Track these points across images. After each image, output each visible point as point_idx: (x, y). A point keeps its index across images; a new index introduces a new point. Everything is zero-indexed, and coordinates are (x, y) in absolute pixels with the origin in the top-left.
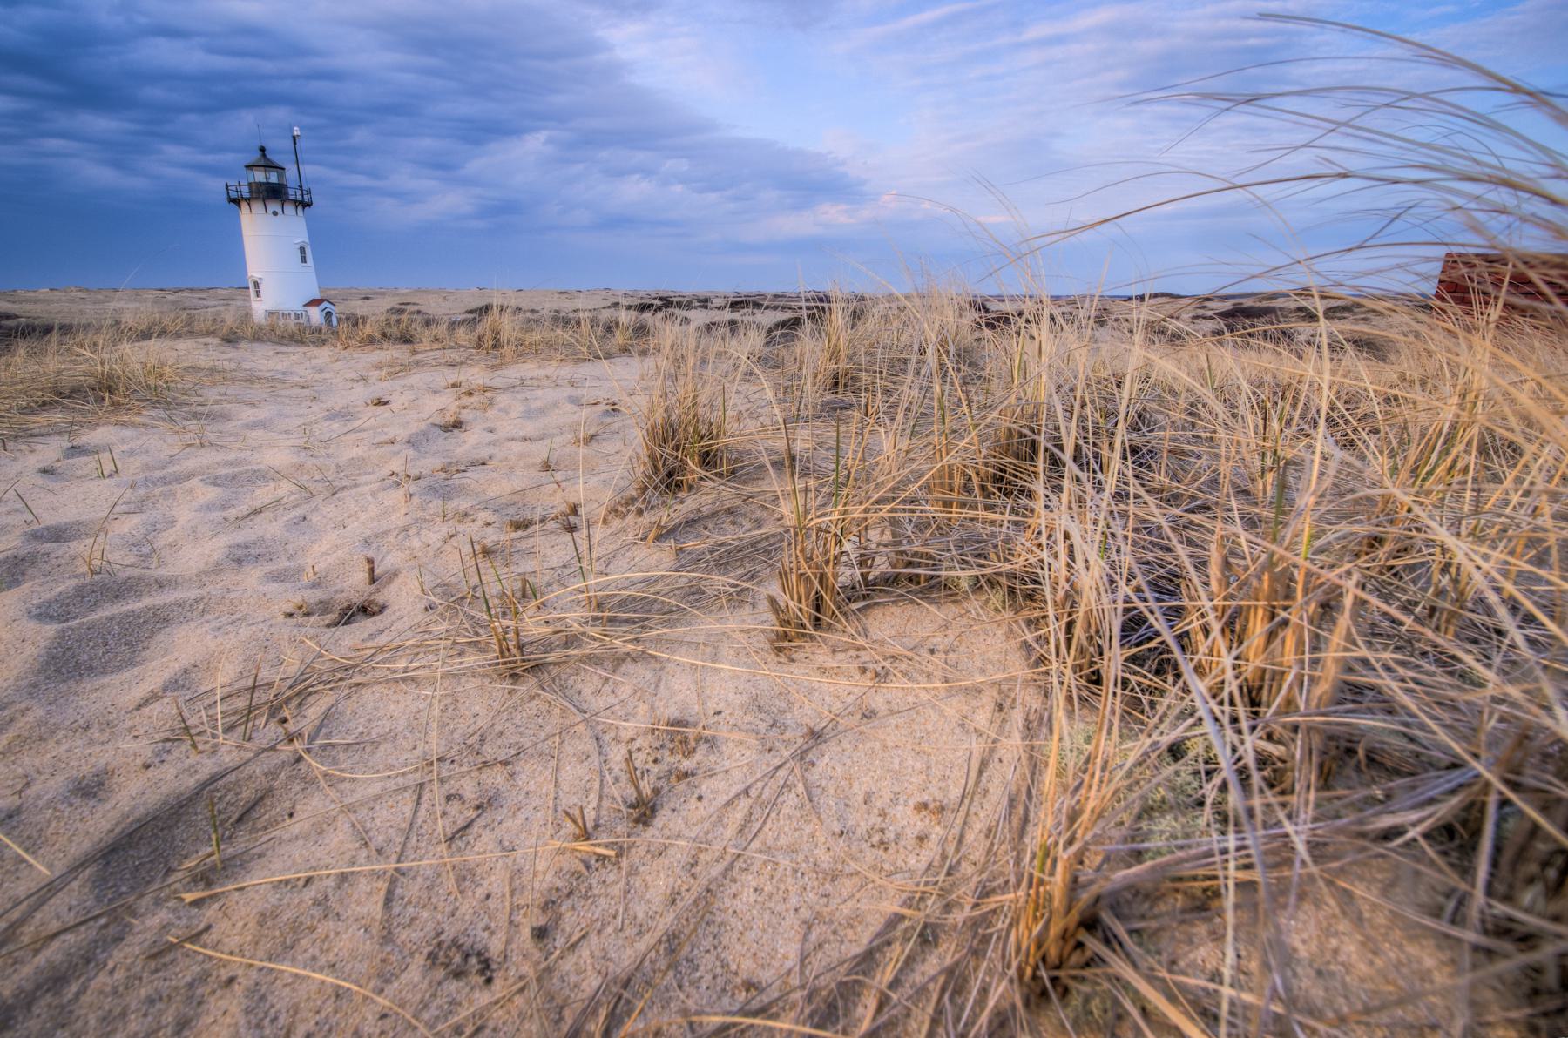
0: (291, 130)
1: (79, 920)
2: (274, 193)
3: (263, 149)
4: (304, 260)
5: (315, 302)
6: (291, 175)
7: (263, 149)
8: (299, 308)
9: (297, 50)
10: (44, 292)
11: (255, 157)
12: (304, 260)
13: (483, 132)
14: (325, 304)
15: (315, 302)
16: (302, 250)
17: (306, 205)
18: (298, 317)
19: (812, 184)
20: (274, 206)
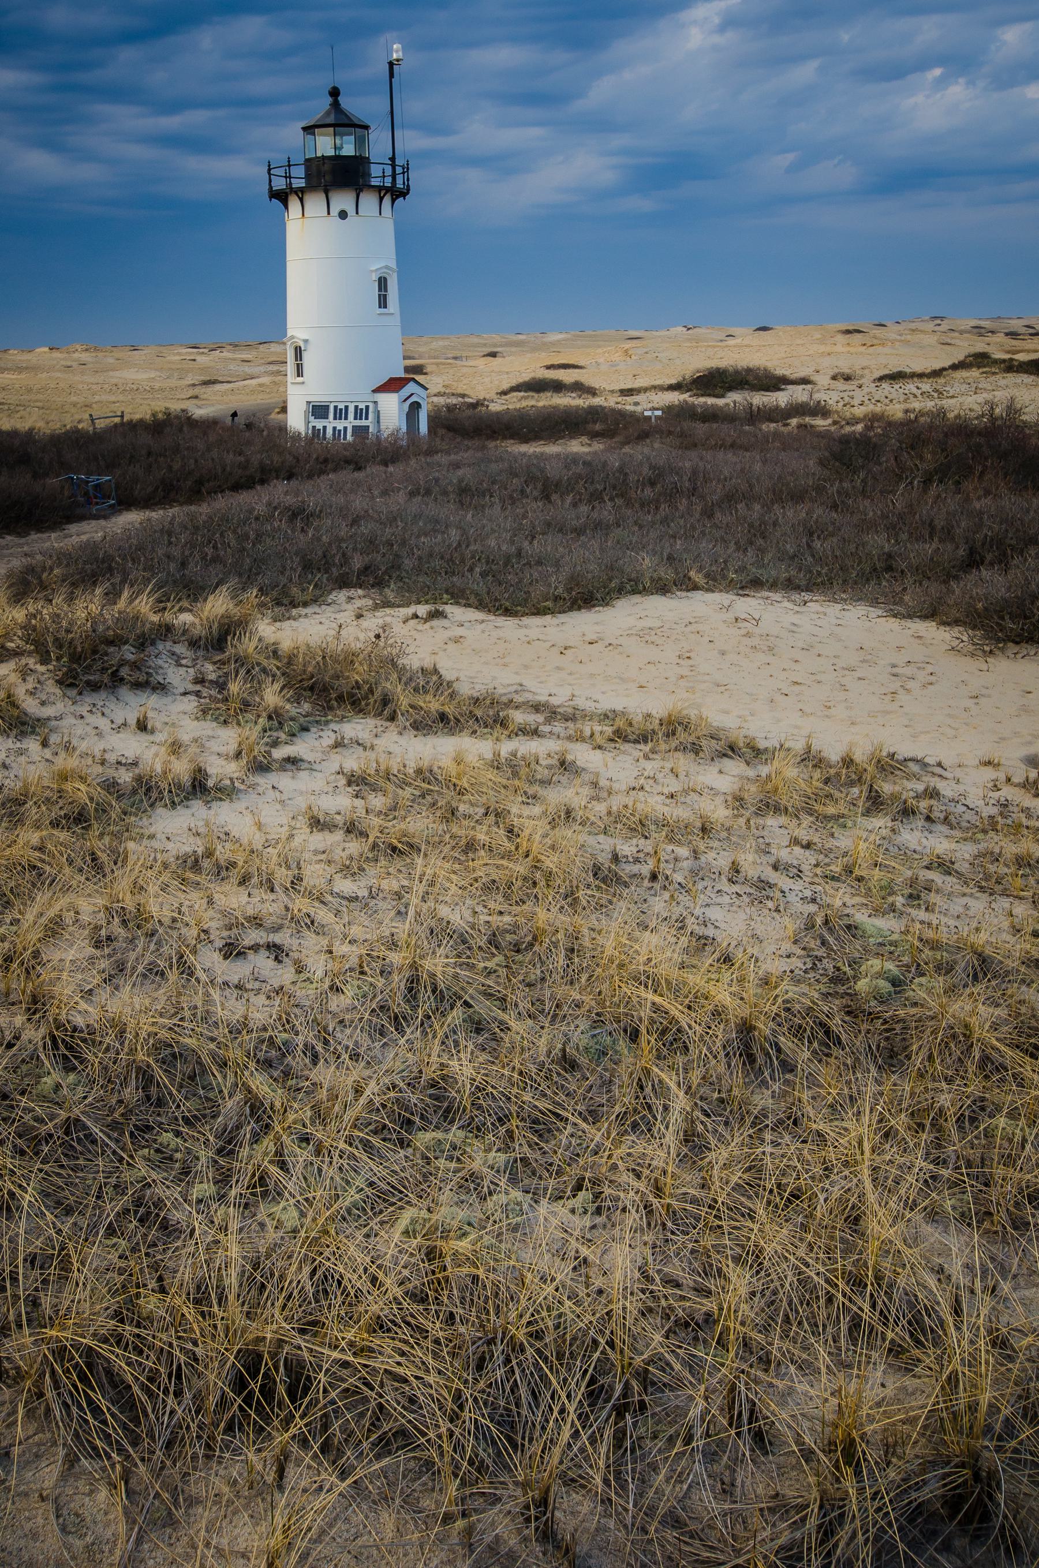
2: (342, 176)
4: (383, 302)
5: (393, 385)
6: (378, 146)
8: (362, 397)
12: (383, 302)
15: (393, 385)
16: (382, 283)
17: (397, 193)
18: (359, 414)
20: (343, 200)
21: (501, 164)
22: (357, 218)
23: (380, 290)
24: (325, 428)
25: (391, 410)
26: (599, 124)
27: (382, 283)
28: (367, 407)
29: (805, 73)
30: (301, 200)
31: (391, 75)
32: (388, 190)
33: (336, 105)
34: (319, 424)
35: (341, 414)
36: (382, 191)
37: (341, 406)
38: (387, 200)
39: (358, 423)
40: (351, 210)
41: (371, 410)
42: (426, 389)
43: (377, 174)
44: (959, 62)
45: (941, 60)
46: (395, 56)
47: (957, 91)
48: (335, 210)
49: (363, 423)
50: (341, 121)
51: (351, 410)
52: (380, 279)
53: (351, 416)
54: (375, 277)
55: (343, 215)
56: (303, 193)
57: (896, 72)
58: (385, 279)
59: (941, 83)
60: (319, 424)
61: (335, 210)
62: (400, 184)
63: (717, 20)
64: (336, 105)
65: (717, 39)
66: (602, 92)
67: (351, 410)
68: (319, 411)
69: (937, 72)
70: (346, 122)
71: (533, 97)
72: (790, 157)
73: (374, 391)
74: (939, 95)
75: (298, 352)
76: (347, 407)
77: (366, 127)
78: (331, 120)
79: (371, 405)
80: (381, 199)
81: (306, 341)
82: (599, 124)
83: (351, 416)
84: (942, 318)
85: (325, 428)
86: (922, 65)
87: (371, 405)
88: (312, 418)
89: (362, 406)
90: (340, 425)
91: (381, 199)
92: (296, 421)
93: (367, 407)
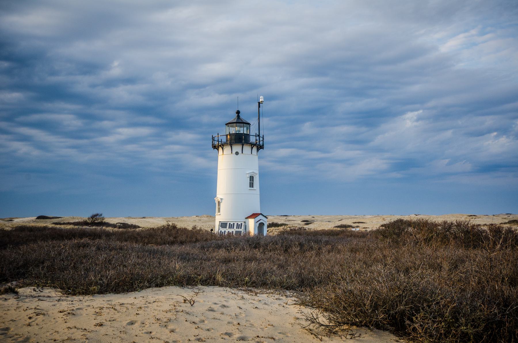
0: (259, 99)
1: (234, 121)
2: (240, 139)
3: (238, 112)
4: (251, 185)
5: (254, 216)
6: (253, 131)
7: (238, 112)
8: (240, 220)
9: (253, 86)
10: (185, 218)
11: (233, 118)
12: (251, 185)
13: (372, 118)
14: (260, 217)
15: (254, 216)
16: (252, 178)
17: (260, 147)
18: (239, 226)
19: (135, 227)
20: (237, 148)
21: (348, 162)
22: (242, 155)
23: (250, 180)
24: (225, 231)
25: (252, 226)
26: (379, 150)
27: (252, 178)
28: (241, 224)
29: (449, 134)
30: (223, 148)
31: (259, 107)
32: (254, 145)
33: (238, 117)
34: (223, 230)
35: (231, 226)
36: (252, 145)
37: (232, 223)
38: (255, 149)
39: (238, 230)
40: (240, 151)
41: (243, 225)
42: (267, 218)
43: (253, 139)
44: (503, 131)
45: (496, 130)
46: (261, 100)
47: (503, 140)
48: (234, 152)
49: (240, 230)
50: (239, 121)
51: (235, 225)
52: (251, 177)
53: (235, 227)
54: (248, 176)
55: (237, 153)
56: (223, 145)
57: (480, 134)
58: (253, 177)
59: (497, 137)
60: (223, 230)
61: (234, 152)
62: (261, 143)
63: (415, 118)
64: (238, 117)
65: (415, 124)
66: (379, 140)
67: (235, 225)
68: (223, 225)
69: (495, 134)
70: (240, 121)
71: (355, 141)
72: (447, 161)
73: (246, 218)
74: (496, 141)
75: (219, 203)
76: (234, 224)
77: (249, 124)
78: (235, 121)
79: (243, 223)
80: (252, 148)
81: (222, 199)
82: (379, 150)
83: (235, 227)
84: (510, 214)
85: (225, 231)
86: (489, 131)
87: (243, 223)
88: (220, 228)
89: (239, 223)
90: (231, 230)
91: (252, 148)
92: (216, 230)
93: (241, 224)
